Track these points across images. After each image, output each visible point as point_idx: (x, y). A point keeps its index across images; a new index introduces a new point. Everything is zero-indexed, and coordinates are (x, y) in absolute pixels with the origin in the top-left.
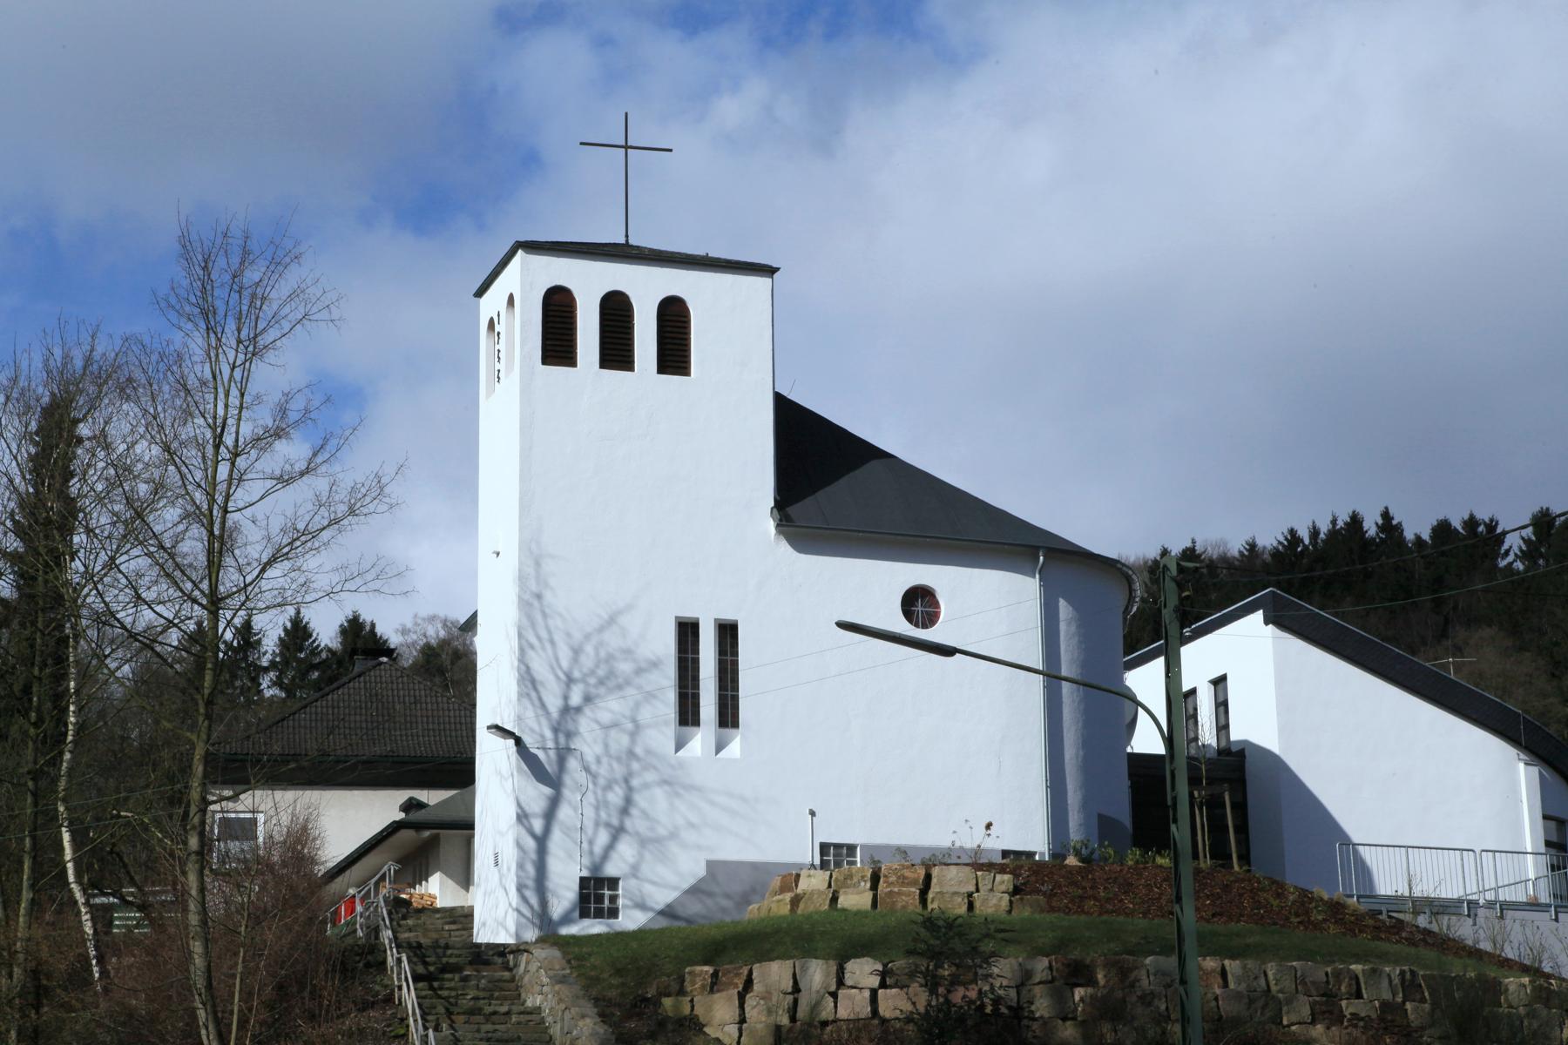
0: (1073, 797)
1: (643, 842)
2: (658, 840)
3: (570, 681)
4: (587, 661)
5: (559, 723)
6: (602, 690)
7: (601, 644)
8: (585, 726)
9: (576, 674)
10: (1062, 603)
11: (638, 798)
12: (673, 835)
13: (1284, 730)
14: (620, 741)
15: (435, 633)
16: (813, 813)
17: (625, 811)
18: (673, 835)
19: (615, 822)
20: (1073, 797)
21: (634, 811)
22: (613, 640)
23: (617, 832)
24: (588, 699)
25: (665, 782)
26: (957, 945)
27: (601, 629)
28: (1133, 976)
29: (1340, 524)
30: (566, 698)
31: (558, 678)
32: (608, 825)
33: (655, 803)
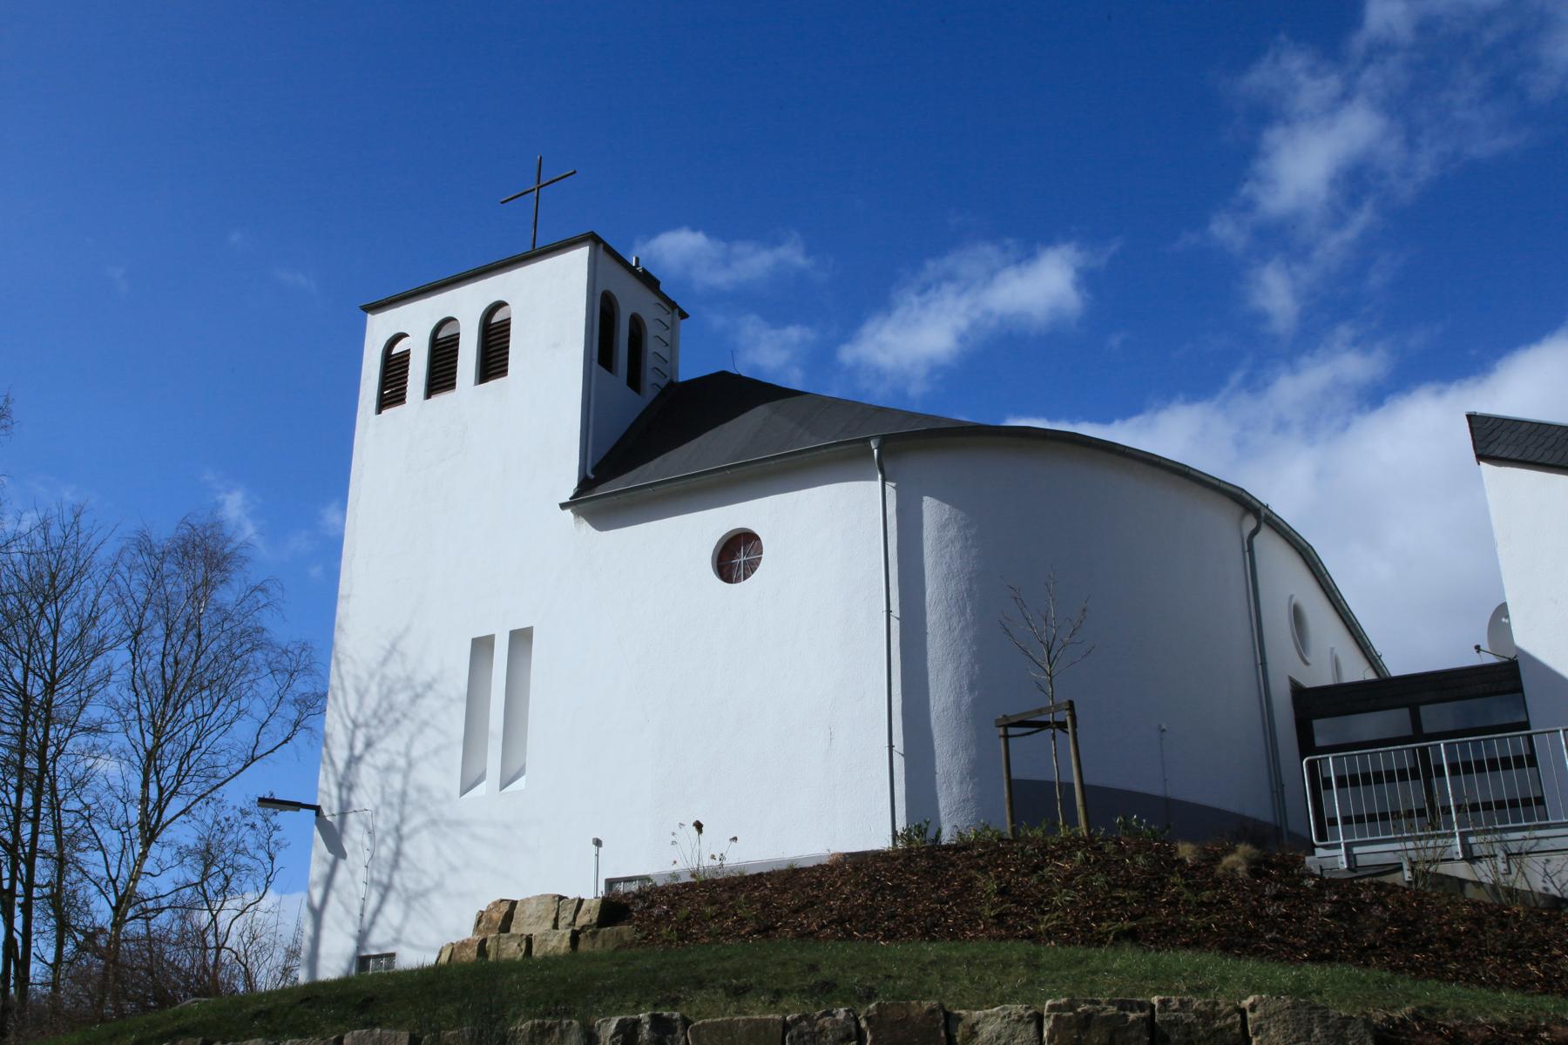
0: (948, 759)
1: (409, 900)
2: (423, 894)
3: (356, 725)
4: (371, 701)
5: (344, 777)
6: (382, 730)
7: (384, 677)
8: (367, 775)
9: (361, 719)
10: (929, 505)
11: (407, 847)
12: (439, 886)
13: (1480, 477)
14: (396, 781)
15: (329, 742)
16: (598, 843)
17: (395, 865)
18: (439, 886)
19: (385, 879)
20: (948, 759)
21: (403, 863)
22: (394, 670)
23: (386, 889)
24: (369, 745)
25: (433, 823)
26: (216, 883)
27: (384, 662)
28: (293, 974)
29: (1355, 366)
30: (351, 747)
31: (345, 726)
32: (379, 883)
33: (422, 849)
